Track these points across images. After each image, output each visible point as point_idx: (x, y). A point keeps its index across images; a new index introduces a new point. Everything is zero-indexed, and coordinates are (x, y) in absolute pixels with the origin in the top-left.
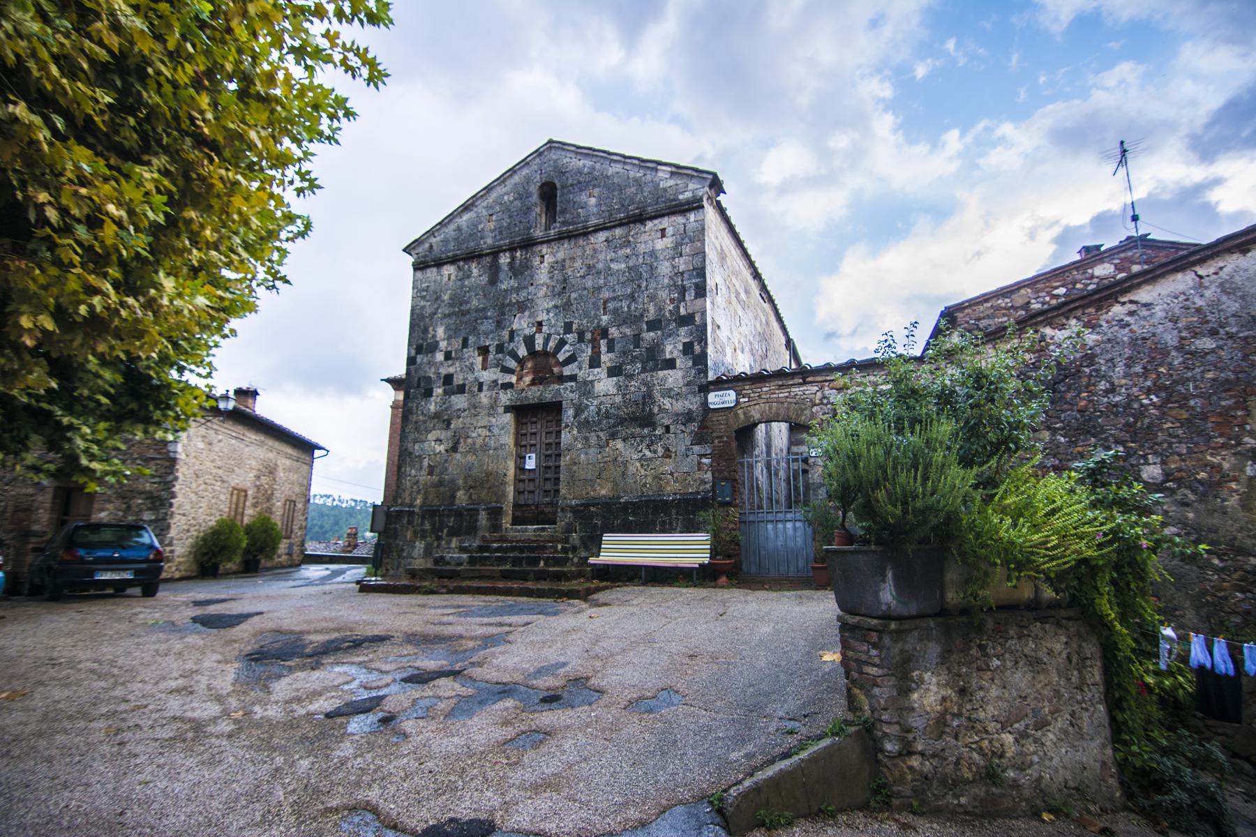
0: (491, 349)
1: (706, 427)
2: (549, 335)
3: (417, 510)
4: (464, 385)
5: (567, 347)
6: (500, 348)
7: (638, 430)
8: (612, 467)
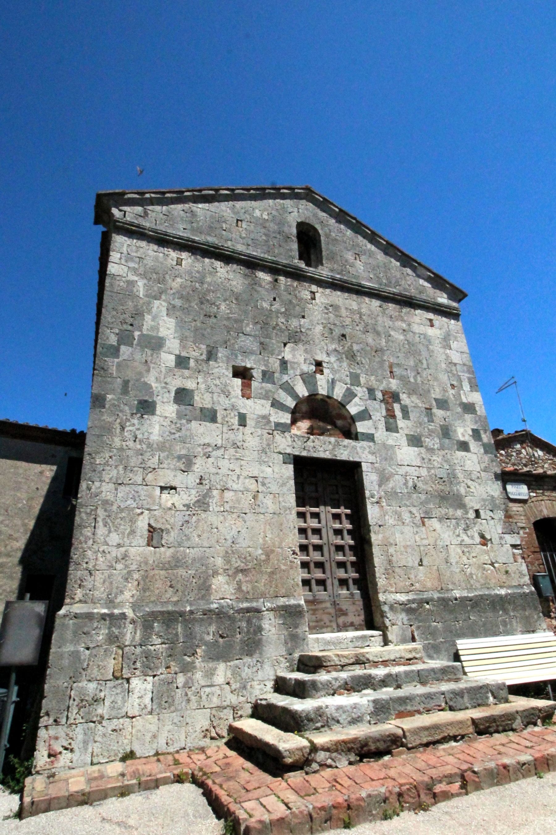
0: (255, 373)
2: (333, 382)
5: (356, 400)
7: (451, 512)
8: (433, 552)
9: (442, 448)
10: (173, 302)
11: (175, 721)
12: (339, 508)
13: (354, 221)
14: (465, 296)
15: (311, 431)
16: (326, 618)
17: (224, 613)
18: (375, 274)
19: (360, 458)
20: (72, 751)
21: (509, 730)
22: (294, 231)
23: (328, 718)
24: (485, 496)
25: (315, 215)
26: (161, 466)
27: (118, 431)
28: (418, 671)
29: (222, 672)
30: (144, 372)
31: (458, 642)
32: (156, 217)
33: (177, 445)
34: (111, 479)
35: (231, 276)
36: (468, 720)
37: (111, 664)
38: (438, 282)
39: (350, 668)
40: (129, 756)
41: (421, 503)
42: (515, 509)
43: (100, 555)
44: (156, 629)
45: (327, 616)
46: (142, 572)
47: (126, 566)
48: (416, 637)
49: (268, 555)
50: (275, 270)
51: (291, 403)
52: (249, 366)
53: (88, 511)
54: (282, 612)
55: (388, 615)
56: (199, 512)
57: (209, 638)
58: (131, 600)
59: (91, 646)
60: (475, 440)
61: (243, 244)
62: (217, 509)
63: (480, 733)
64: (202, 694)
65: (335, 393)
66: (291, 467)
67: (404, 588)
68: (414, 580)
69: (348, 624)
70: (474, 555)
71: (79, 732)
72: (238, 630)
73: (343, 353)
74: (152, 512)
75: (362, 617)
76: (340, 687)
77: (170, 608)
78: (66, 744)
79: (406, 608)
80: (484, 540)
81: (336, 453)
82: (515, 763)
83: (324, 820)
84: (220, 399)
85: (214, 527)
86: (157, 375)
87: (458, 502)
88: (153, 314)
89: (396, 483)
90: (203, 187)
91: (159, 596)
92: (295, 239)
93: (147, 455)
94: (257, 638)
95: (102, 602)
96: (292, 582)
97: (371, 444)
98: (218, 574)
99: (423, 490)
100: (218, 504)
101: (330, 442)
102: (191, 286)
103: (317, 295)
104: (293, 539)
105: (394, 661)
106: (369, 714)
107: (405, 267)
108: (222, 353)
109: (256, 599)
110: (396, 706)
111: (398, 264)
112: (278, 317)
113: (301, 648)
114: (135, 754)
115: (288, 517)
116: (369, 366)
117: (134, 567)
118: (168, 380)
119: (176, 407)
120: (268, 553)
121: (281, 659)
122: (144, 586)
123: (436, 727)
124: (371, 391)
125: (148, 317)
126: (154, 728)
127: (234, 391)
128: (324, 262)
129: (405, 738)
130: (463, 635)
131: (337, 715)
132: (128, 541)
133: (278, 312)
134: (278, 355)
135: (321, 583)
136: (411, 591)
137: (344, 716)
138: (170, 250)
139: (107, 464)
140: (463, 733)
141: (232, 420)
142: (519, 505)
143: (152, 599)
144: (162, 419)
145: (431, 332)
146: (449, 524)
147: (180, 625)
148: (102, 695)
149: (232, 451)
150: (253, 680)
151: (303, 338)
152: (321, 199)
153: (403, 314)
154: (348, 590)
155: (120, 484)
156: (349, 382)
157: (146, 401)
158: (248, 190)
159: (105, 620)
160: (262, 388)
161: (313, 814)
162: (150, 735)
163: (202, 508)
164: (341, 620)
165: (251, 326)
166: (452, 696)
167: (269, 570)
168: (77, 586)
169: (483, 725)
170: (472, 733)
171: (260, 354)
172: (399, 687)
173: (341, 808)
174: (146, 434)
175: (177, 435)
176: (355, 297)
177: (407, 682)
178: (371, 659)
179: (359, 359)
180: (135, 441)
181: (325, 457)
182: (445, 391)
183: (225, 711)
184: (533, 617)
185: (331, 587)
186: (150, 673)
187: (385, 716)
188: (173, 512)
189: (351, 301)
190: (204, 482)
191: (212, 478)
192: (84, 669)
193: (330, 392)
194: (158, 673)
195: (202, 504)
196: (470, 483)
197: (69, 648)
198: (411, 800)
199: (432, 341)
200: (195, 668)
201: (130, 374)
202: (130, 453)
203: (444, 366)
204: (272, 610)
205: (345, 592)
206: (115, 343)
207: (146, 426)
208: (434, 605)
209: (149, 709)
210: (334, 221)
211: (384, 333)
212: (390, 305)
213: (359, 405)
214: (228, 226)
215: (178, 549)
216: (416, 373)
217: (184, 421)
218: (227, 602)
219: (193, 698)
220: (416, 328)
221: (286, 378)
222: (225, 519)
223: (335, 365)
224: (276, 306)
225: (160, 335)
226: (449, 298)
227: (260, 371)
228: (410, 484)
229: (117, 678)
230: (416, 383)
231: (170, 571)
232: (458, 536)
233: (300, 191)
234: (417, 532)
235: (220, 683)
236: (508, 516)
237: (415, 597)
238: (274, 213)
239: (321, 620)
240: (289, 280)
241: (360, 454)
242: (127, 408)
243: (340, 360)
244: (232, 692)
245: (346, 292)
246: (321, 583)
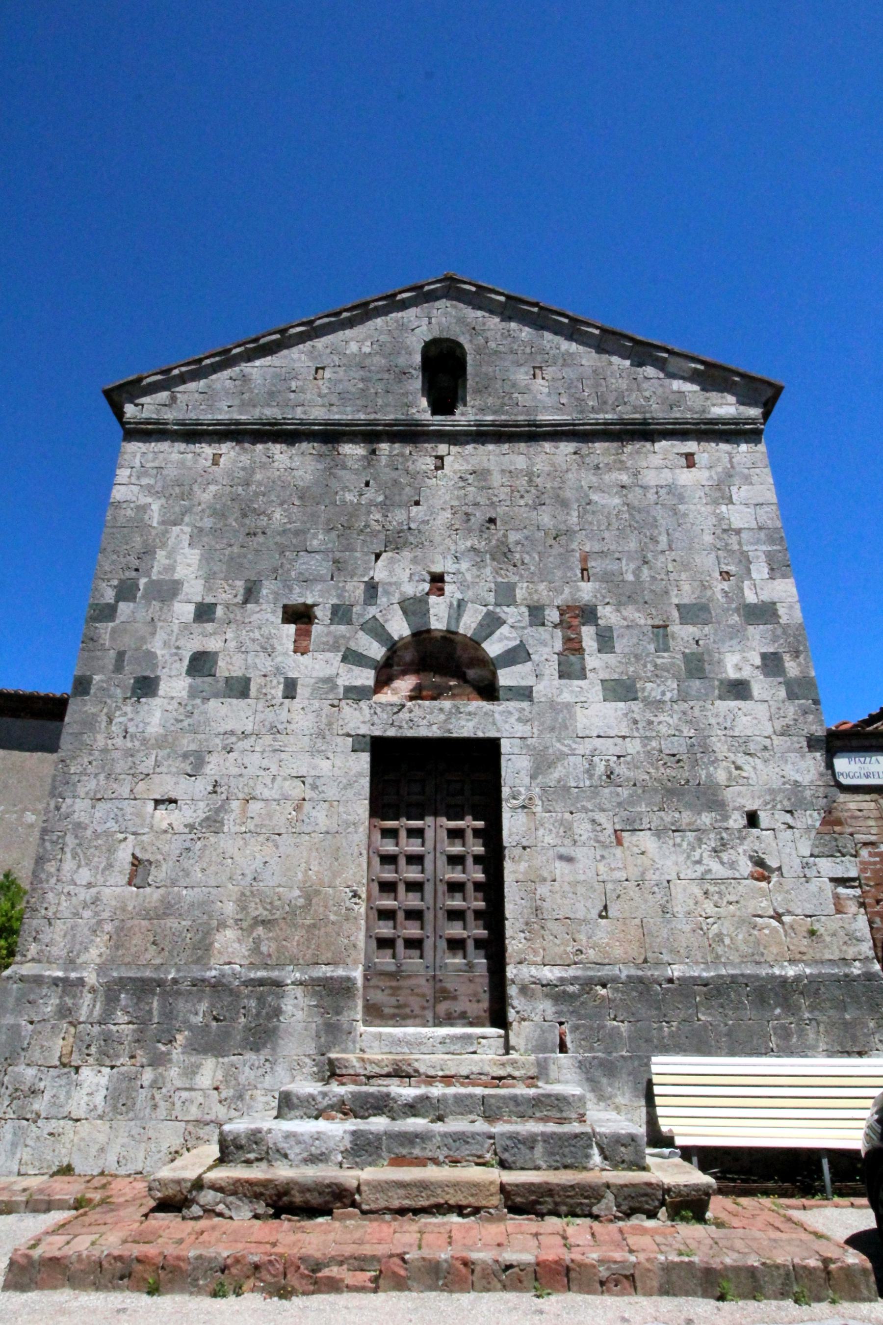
0: (318, 612)
1: (839, 822)
2: (461, 604)
3: (91, 978)
4: (247, 681)
5: (504, 630)
6: (341, 614)
7: (686, 817)
8: (633, 892)
9: (683, 696)
11: (133, 1133)
12: (462, 819)
13: (536, 310)
15: (417, 695)
16: (415, 1003)
17: (223, 985)
18: (571, 396)
19: (498, 730)
21: (585, 1216)
22: (418, 359)
23: (268, 1148)
24: (776, 784)
25: (461, 321)
26: (158, 770)
27: (104, 724)
28: (483, 1097)
29: (210, 1070)
30: (148, 636)
32: (191, 402)
33: (183, 738)
34: (87, 793)
36: (492, 1183)
37: (58, 1046)
38: (714, 377)
39: (380, 1082)
40: (67, 1170)
41: (619, 804)
43: (63, 898)
44: (123, 1003)
45: (418, 999)
46: (116, 923)
47: (96, 914)
48: (569, 1045)
49: (309, 899)
50: (370, 435)
51: (377, 652)
52: (309, 601)
53: (55, 838)
54: (317, 988)
55: (515, 1003)
56: (207, 835)
58: (98, 961)
59: (36, 1019)
60: (766, 675)
61: (323, 406)
62: (234, 829)
63: (516, 1209)
64: (176, 1099)
65: (461, 624)
67: (561, 958)
68: (584, 942)
69: (456, 1015)
70: (732, 898)
72: (242, 1011)
73: (486, 552)
74: (139, 837)
75: (485, 1005)
76: (332, 1107)
77: (148, 973)
81: (451, 727)
82: (490, 1262)
83: (118, 1275)
84: (257, 661)
85: (227, 856)
86: (166, 637)
87: (710, 798)
88: (169, 548)
89: (572, 770)
90: (259, 334)
92: (418, 374)
95: (61, 961)
96: (346, 941)
97: (525, 705)
98: (226, 926)
99: (628, 779)
100: (238, 821)
101: (441, 709)
102: (231, 492)
103: (448, 460)
104: (355, 874)
105: (467, 1077)
106: (342, 1152)
107: (640, 365)
108: (267, 589)
109: (280, 966)
111: (628, 363)
112: (369, 513)
113: (343, 1046)
114: (73, 1169)
117: (106, 915)
118: (180, 643)
119: (189, 680)
120: (310, 895)
121: (307, 1060)
122: (119, 940)
123: (423, 1186)
124: (536, 613)
125: (161, 554)
126: (102, 1138)
127: (281, 644)
128: (468, 399)
129: (360, 1195)
130: (664, 1049)
131: (285, 1145)
132: (102, 880)
133: (372, 503)
134: (364, 576)
135: (414, 944)
136: (575, 963)
138: (203, 445)
139: (84, 773)
140: (476, 1204)
141: (273, 691)
142: (867, 797)
143: (127, 960)
144: (166, 701)
145: (686, 477)
146: (678, 840)
147: (156, 998)
148: (42, 1085)
149: (268, 739)
150: (256, 1088)
151: (411, 539)
152: (473, 289)
153: (624, 458)
154: (394, 957)
155: (100, 799)
156: (492, 600)
157: (146, 678)
158: (337, 314)
159: (57, 986)
160: (329, 633)
161: (104, 1263)
162: (97, 1147)
163: (212, 829)
165: (321, 537)
166: (509, 1142)
167: (307, 922)
168: (31, 939)
169: (523, 1196)
170: (496, 1207)
171: (332, 579)
172: (440, 1118)
173: (149, 1264)
174: (141, 725)
175: (186, 723)
176: (522, 446)
178: (422, 1070)
179: (518, 556)
180: (125, 737)
181: (430, 735)
183: (207, 1127)
185: (431, 953)
186: (108, 1063)
187: (370, 1159)
188: (169, 836)
189: (513, 457)
190: (219, 789)
191: (233, 782)
192: (23, 1049)
193: (453, 622)
194: (118, 1064)
195: (213, 822)
196: (741, 759)
198: (269, 1278)
201: (127, 642)
202: (116, 755)
203: (708, 538)
204: (301, 984)
206: (112, 601)
207: (142, 713)
209: (100, 1111)
210: (497, 320)
211: (578, 500)
212: (597, 445)
213: (507, 638)
214: (300, 383)
215: (170, 889)
217: (198, 701)
218: (233, 969)
219: (162, 1104)
220: (650, 478)
221: (372, 611)
222: (246, 844)
223: (469, 577)
224: (370, 494)
225: (177, 576)
226: (741, 402)
227: (328, 606)
228: (601, 768)
229: (64, 1065)
231: (155, 921)
232: (699, 862)
233: (432, 287)
234: (603, 857)
235: (203, 1087)
236: (831, 820)
238: (382, 338)
239: (405, 1006)
240: (397, 445)
241: (500, 723)
242: (119, 691)
243: (479, 565)
244: (220, 1102)
245: (504, 442)
246: (414, 944)
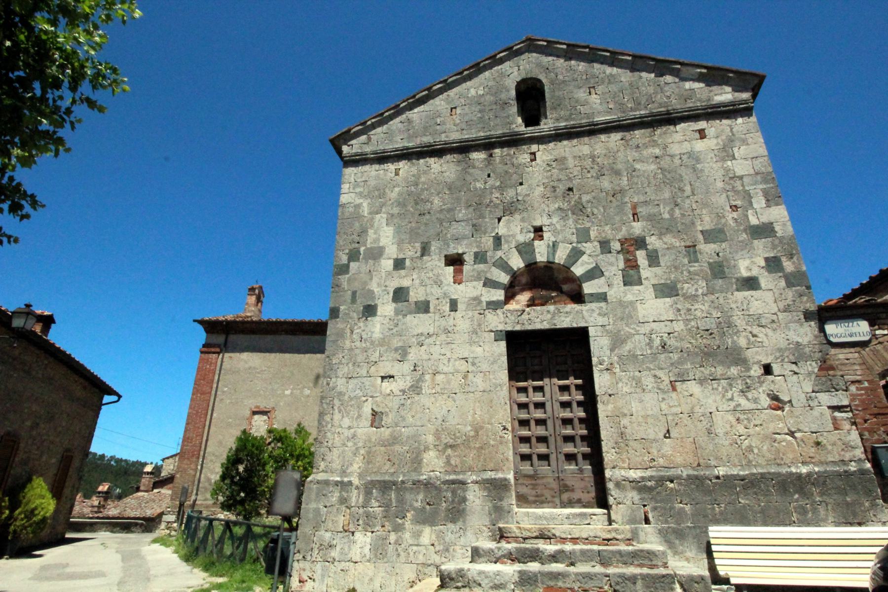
0: (466, 257)
5: (585, 258)
7: (720, 370)
9: (711, 291)
10: (391, 212)
13: (587, 50)
14: (761, 78)
15: (532, 303)
16: (548, 494)
18: (615, 103)
19: (586, 322)
20: (314, 580)
24: (783, 344)
27: (349, 334)
29: (428, 534)
31: (710, 528)
35: (445, 168)
37: (341, 520)
38: (714, 76)
42: (841, 356)
46: (366, 449)
47: (355, 444)
49: (477, 432)
51: (505, 278)
52: (460, 251)
55: (613, 493)
57: (418, 505)
58: (358, 471)
60: (770, 272)
62: (428, 392)
66: (503, 344)
67: (640, 464)
70: (758, 422)
71: (318, 567)
75: (593, 494)
76: (504, 556)
77: (387, 478)
78: (310, 575)
79: (639, 486)
80: (777, 403)
84: (432, 290)
87: (736, 357)
89: (636, 344)
91: (380, 468)
93: (370, 352)
94: (461, 508)
99: (676, 348)
101: (548, 312)
105: (587, 539)
107: (662, 76)
109: (463, 472)
110: (545, 580)
112: (492, 193)
115: (498, 393)
116: (603, 215)
117: (360, 444)
118: (387, 283)
119: (394, 305)
120: (477, 429)
121: (484, 528)
122: (369, 458)
125: (371, 232)
126: (370, 573)
130: (717, 522)
133: (493, 187)
135: (544, 457)
136: (651, 467)
137: (486, 581)
139: (340, 363)
142: (852, 350)
145: (700, 146)
146: (715, 386)
148: (335, 542)
149: (443, 337)
151: (520, 207)
157: (369, 306)
158: (461, 73)
162: (368, 578)
164: (565, 496)
167: (477, 446)
172: (572, 564)
175: (394, 331)
176: (586, 139)
177: (581, 561)
178: (557, 535)
182: (720, 216)
184: (862, 504)
190: (417, 368)
193: (551, 256)
195: (416, 388)
196: (756, 330)
197: (313, 505)
199: (701, 157)
200: (404, 529)
201: (356, 285)
205: (573, 467)
208: (680, 484)
209: (368, 557)
210: (562, 61)
214: (442, 119)
216: (672, 206)
217: (400, 317)
219: (402, 553)
221: (499, 254)
224: (491, 181)
225: (381, 244)
226: (734, 90)
228: (657, 342)
230: (672, 218)
234: (664, 399)
236: (826, 366)
237: (654, 474)
238: (490, 84)
239: (542, 495)
240: (505, 149)
246: (544, 457)
